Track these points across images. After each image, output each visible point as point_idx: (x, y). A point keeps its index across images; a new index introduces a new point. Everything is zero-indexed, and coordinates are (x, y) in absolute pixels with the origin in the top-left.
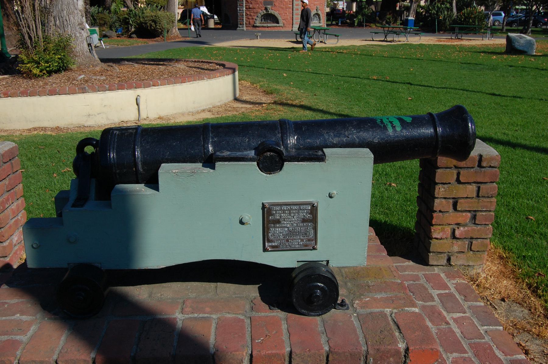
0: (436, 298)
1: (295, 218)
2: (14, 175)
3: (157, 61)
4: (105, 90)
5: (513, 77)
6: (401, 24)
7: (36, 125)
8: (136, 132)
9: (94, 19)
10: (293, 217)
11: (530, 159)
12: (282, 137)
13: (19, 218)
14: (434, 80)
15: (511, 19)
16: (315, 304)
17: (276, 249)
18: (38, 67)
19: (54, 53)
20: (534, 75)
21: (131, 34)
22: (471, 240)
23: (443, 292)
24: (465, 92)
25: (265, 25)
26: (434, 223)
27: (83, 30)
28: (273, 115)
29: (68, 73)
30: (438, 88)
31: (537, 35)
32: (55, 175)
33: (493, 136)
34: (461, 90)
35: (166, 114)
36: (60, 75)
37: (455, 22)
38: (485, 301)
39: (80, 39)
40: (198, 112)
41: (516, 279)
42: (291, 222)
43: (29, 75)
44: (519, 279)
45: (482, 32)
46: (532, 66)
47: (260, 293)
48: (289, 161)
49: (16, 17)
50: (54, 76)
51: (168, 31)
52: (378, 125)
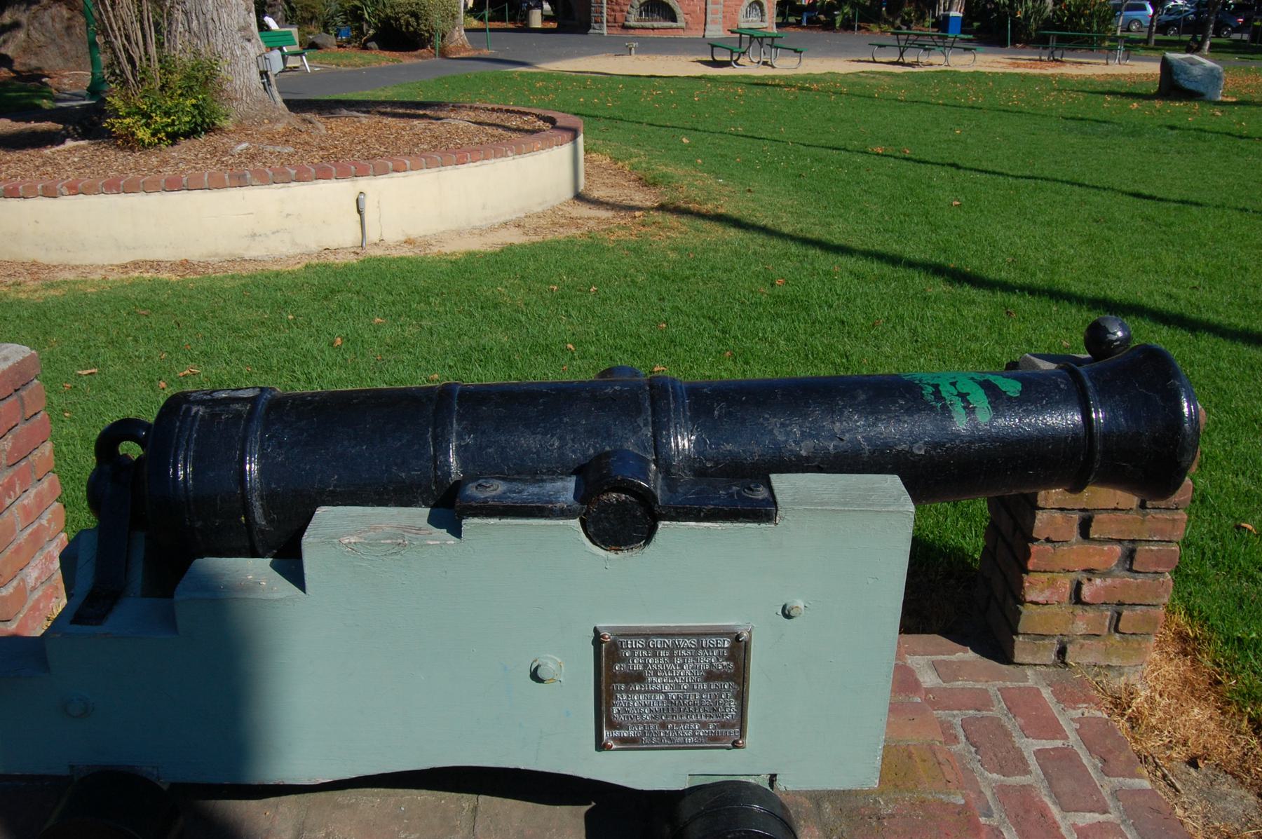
0: (1033, 762)
2: (28, 424)
3: (411, 109)
4: (288, 180)
5: (1179, 153)
6: (934, 25)
7: (139, 256)
8: (251, 413)
9: (292, 9)
10: (681, 666)
11: (1232, 363)
12: (654, 436)
13: (44, 522)
14: (1008, 158)
15: (1164, 17)
17: (629, 743)
18: (147, 125)
19: (181, 95)
20: (1222, 150)
21: (367, 41)
22: (1118, 608)
23: (1049, 744)
24: (1076, 188)
25: (648, 24)
26: (1030, 568)
27: (249, 40)
28: (656, 239)
29: (214, 138)
30: (1017, 177)
31: (1223, 56)
32: (163, 384)
33: (1145, 300)
34: (1067, 182)
35: (423, 233)
36: (197, 143)
37: (1048, 24)
38: (1151, 768)
39: (242, 62)
40: (492, 229)
41: (1224, 705)
42: (672, 679)
43: (128, 142)
44: (1229, 703)
45: (1106, 48)
46: (1217, 128)
48: (671, 519)
49: (101, 14)
50: (184, 143)
51: (443, 36)
52: (927, 403)
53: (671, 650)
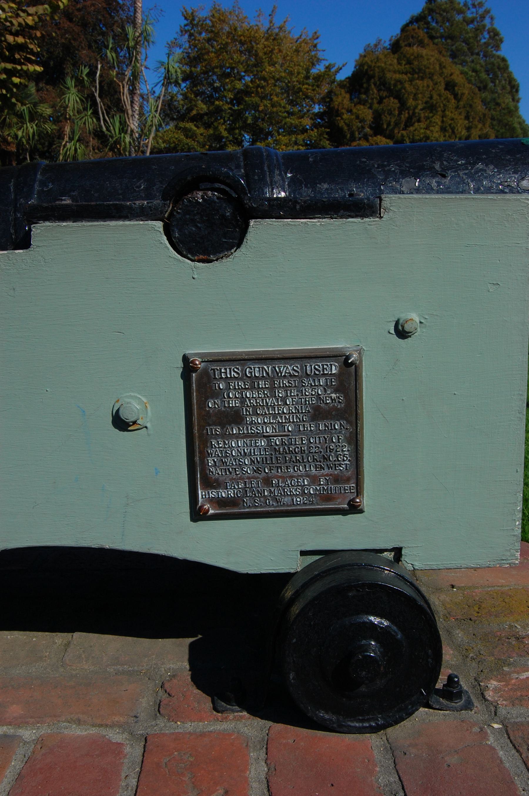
1: (291, 405)
16: (363, 689)
17: (231, 510)
42: (275, 417)
47: (191, 661)
53: (270, 378)
